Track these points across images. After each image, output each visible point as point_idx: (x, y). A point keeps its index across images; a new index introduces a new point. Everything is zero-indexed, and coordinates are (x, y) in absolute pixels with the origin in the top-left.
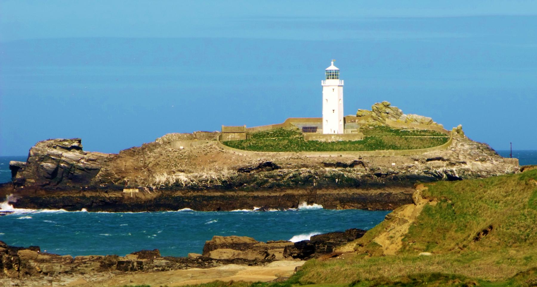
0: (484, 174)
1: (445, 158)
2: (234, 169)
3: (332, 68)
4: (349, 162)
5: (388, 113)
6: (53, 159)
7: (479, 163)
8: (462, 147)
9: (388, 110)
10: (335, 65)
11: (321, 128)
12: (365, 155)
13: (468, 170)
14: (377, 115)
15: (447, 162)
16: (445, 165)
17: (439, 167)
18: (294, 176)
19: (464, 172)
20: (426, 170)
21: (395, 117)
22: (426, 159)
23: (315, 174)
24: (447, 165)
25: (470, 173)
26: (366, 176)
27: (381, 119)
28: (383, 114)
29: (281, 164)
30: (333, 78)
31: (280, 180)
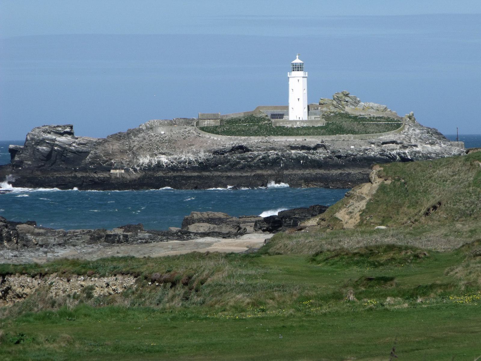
0: (433, 155)
1: (399, 141)
2: (209, 151)
3: (297, 61)
4: (312, 145)
5: (347, 102)
6: (48, 143)
7: (429, 146)
8: (414, 132)
9: (347, 99)
10: (299, 58)
11: (288, 114)
12: (327, 139)
13: (419, 152)
14: (337, 103)
15: (400, 145)
16: (398, 148)
17: (393, 150)
18: (264, 158)
19: (415, 154)
20: (382, 153)
21: (353, 105)
22: (382, 142)
23: (282, 156)
24: (400, 148)
25: (421, 155)
26: (328, 157)
27: (341, 106)
28: (343, 103)
29: (252, 147)
30: (298, 70)
31: (250, 161)
